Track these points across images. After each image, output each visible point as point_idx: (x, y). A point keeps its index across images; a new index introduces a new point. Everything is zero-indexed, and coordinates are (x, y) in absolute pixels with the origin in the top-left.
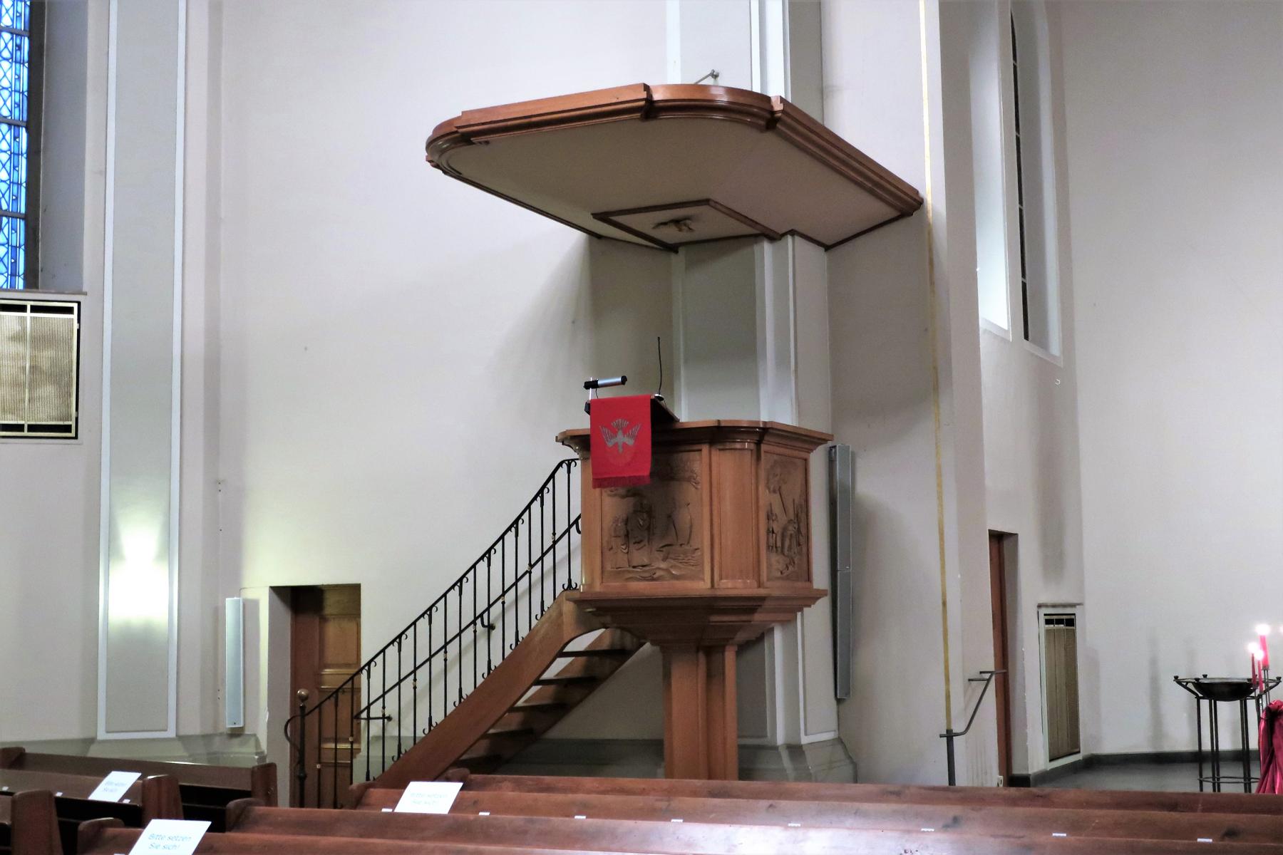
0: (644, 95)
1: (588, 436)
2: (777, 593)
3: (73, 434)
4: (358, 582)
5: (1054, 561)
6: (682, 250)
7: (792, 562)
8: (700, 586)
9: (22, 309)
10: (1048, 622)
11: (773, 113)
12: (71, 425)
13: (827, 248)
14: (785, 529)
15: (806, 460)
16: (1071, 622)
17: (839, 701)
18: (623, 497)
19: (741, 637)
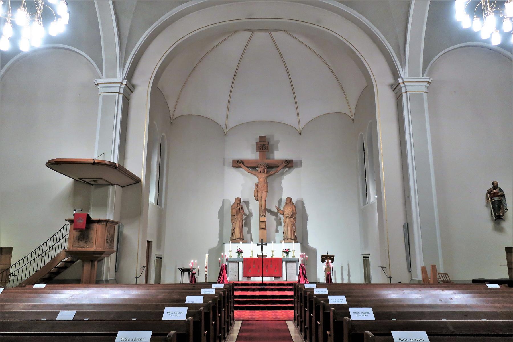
0: (93, 161)
1: (73, 220)
2: (107, 251)
5: (159, 246)
6: (94, 185)
7: (110, 245)
8: (92, 249)
10: (157, 258)
11: (116, 166)
13: (122, 187)
14: (110, 239)
15: (115, 227)
16: (161, 258)
17: (116, 272)
18: (78, 232)
19: (99, 259)
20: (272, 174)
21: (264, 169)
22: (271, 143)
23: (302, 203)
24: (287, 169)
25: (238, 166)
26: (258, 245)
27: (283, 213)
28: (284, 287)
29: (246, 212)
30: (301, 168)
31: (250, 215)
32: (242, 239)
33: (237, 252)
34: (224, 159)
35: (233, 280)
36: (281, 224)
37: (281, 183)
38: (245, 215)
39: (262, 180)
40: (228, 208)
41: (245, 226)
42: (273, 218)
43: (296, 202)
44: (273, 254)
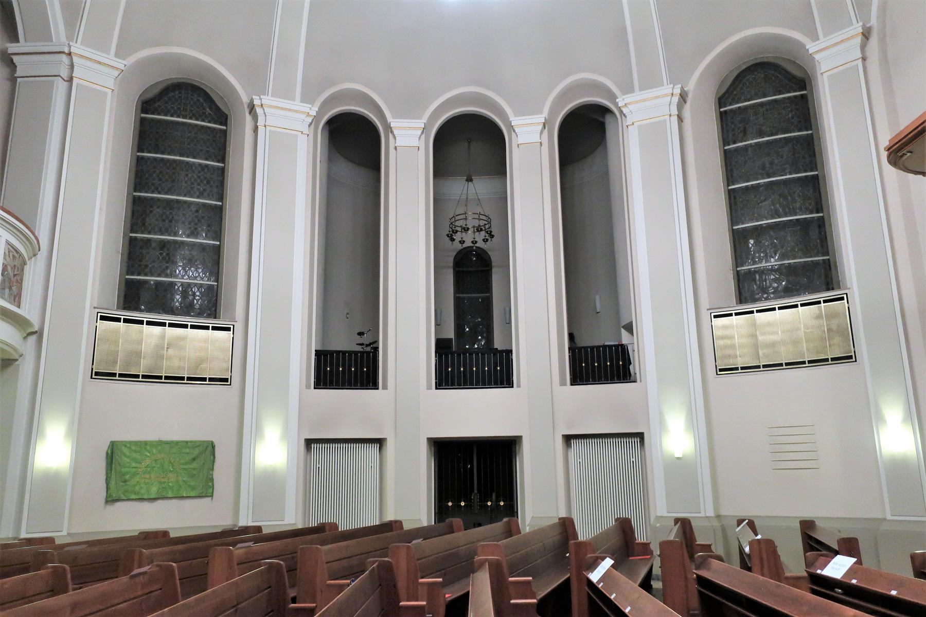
3: (229, 383)
4: (426, 441)
9: (819, 303)
12: (228, 378)
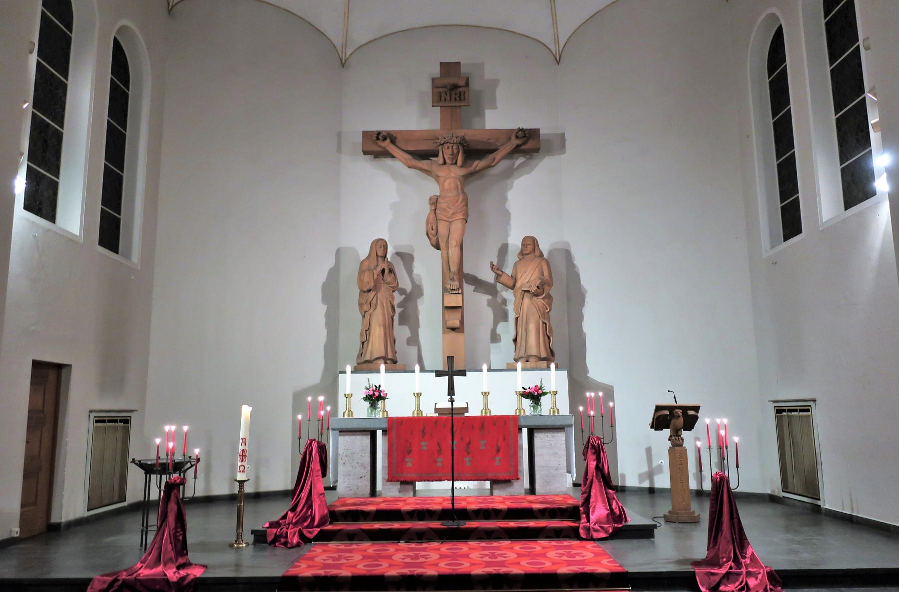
16: (126, 421)
20: (477, 169)
21: (455, 151)
22: (476, 85)
23: (568, 254)
24: (521, 160)
25: (379, 149)
26: (439, 374)
27: (511, 284)
28: (532, 524)
29: (405, 283)
30: (563, 156)
31: (417, 291)
32: (394, 364)
33: (366, 399)
34: (339, 135)
35: (351, 492)
36: (505, 317)
37: (505, 199)
38: (402, 292)
39: (450, 184)
40: (350, 271)
41: (401, 323)
42: (484, 298)
43: (551, 253)
44: (418, 406)
